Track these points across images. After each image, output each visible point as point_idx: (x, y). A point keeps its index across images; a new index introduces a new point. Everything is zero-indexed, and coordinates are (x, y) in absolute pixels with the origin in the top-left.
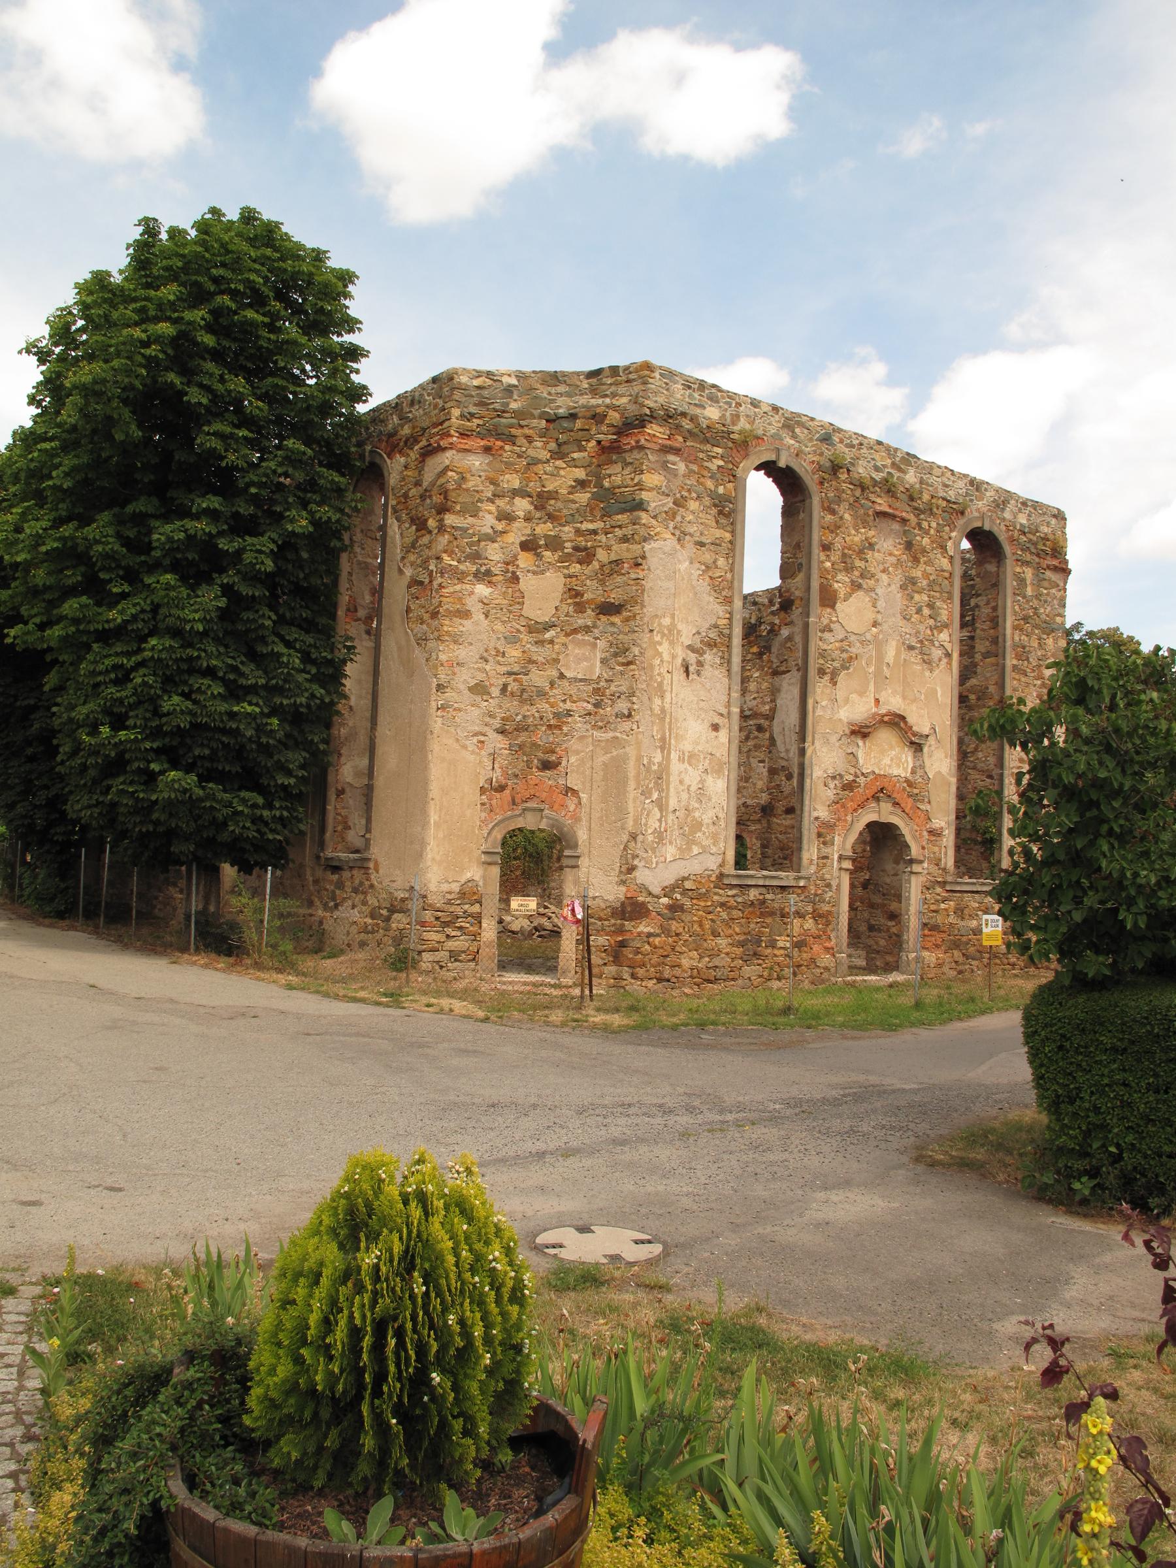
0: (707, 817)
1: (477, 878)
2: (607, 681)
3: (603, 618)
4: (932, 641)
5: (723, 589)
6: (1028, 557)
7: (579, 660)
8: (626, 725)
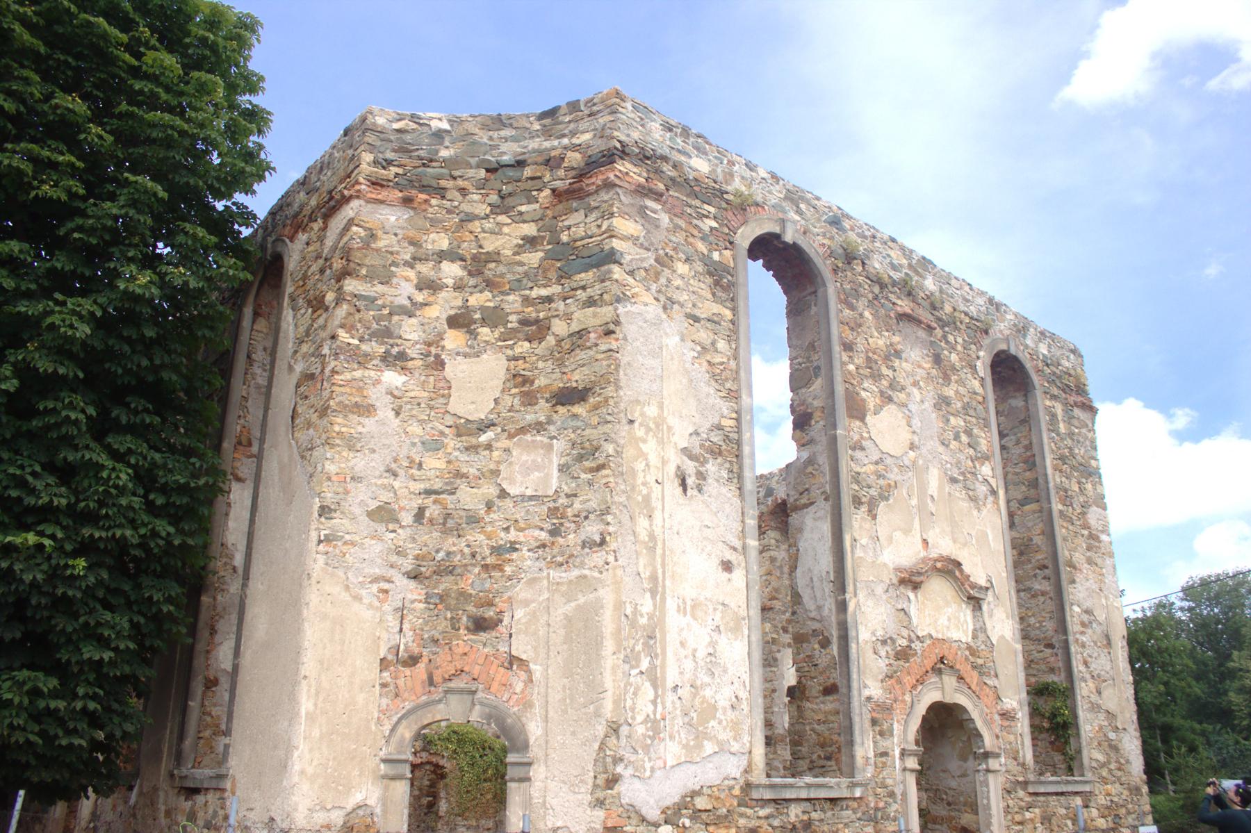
0: (723, 698)
1: (371, 802)
2: (568, 496)
3: (560, 409)
4: (974, 474)
5: (727, 380)
6: (1055, 391)
7: (527, 471)
8: (598, 557)
